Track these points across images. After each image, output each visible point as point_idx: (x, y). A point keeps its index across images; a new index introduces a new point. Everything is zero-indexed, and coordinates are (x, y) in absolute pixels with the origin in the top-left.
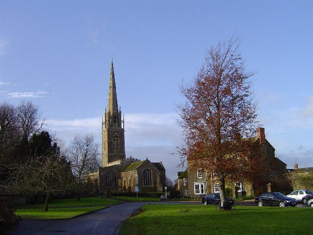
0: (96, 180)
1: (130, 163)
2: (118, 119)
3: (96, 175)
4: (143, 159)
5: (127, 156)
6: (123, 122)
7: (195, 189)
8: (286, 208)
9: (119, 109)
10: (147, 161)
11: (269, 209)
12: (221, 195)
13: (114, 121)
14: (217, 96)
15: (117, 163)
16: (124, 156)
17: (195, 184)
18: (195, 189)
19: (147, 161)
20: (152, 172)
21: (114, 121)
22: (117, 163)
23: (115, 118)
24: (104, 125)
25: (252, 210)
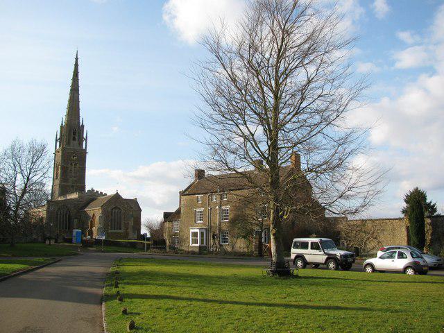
0: (37, 153)
1: (94, 196)
2: (79, 136)
3: (42, 212)
4: (110, 192)
5: (88, 188)
6: (86, 140)
7: (273, 249)
8: (416, 276)
9: (81, 121)
10: (117, 196)
11: (341, 274)
12: (120, 231)
13: (72, 136)
14: (266, 87)
15: (74, 196)
16: (84, 187)
17: (192, 231)
18: (273, 249)
19: (117, 196)
20: (123, 211)
21: (72, 136)
22: (74, 196)
23: (74, 134)
24: (58, 143)
25: (92, 227)
